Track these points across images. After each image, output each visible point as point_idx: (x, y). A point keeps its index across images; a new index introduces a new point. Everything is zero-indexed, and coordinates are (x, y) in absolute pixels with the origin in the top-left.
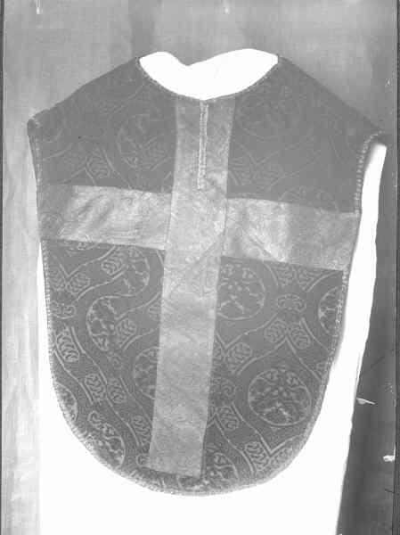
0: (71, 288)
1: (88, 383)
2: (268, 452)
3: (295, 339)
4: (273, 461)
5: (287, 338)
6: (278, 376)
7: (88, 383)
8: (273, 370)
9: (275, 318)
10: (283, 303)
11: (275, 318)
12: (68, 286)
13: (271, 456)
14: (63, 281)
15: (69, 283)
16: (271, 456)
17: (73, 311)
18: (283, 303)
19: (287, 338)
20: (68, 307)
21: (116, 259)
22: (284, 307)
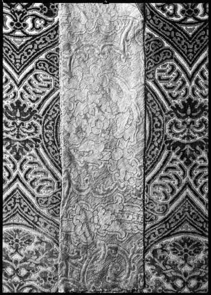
0: (26, 96)
1: (160, 78)
2: (192, 189)
3: (179, 75)
4: (184, 176)
5: (190, 72)
6: (25, 25)
7: (160, 78)
8: (34, 32)
9: (39, 108)
10: (30, 128)
11: (39, 108)
12: (22, 94)
13: (188, 184)
14: (12, 87)
15: (21, 89)
16: (188, 184)
17: (36, 128)
18: (30, 128)
19: (190, 72)
20: (27, 124)
21: (171, 173)
22: (27, 124)
